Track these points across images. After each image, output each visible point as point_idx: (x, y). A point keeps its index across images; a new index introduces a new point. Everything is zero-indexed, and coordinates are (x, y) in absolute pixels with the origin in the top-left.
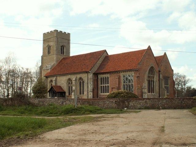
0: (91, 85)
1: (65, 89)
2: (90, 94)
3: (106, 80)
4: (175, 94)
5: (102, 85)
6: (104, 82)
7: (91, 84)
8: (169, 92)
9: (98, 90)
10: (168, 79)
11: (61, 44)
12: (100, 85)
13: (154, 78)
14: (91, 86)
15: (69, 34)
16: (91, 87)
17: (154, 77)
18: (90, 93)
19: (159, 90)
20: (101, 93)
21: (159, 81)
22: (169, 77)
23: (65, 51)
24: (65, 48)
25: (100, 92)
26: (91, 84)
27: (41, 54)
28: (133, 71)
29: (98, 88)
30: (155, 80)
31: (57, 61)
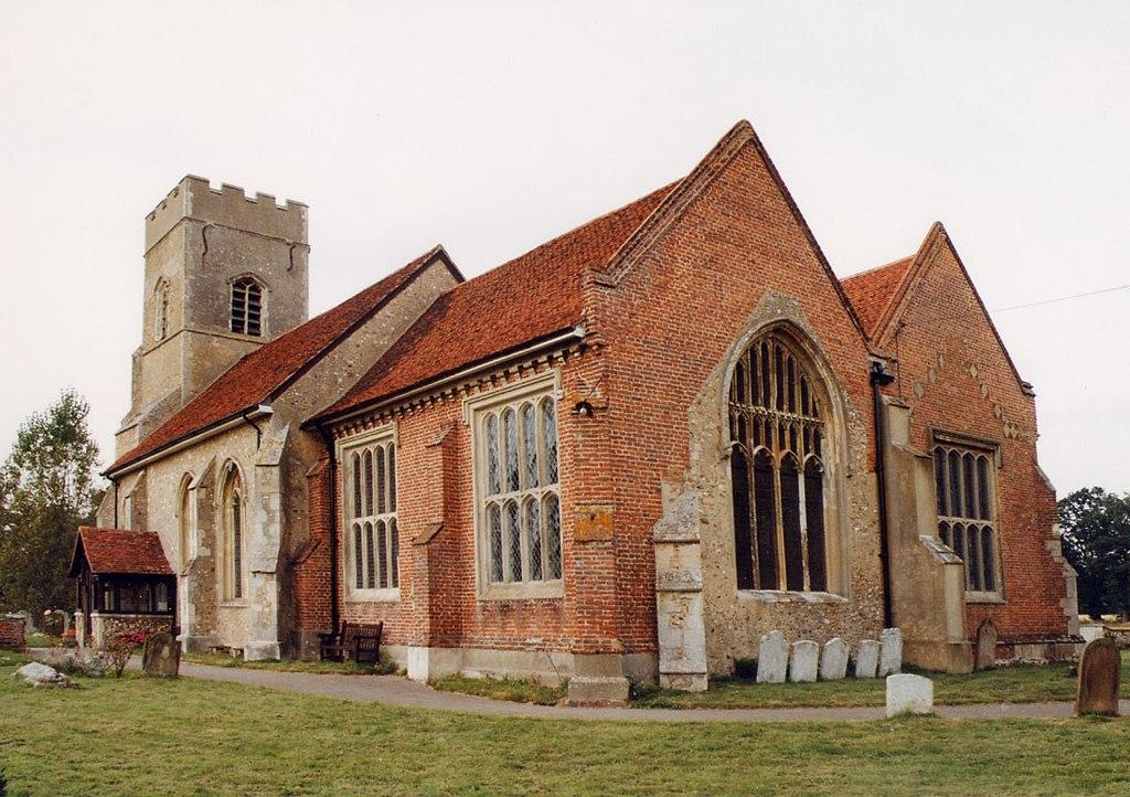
0: (271, 520)
1: (180, 548)
2: (261, 595)
3: (379, 466)
4: (1063, 593)
5: (361, 521)
6: (375, 506)
7: (266, 507)
8: (998, 579)
9: (334, 560)
10: (982, 461)
11: (236, 271)
12: (348, 522)
13: (814, 438)
14: (266, 526)
15: (296, 210)
16: (266, 534)
17: (818, 437)
18: (260, 581)
19: (885, 557)
20: (360, 585)
21: (879, 467)
22: (990, 447)
23: (264, 314)
24: (264, 294)
25: (353, 581)
26: (266, 507)
27: (135, 340)
28: (551, 361)
29: (335, 543)
30: (831, 460)
31: (198, 375)
